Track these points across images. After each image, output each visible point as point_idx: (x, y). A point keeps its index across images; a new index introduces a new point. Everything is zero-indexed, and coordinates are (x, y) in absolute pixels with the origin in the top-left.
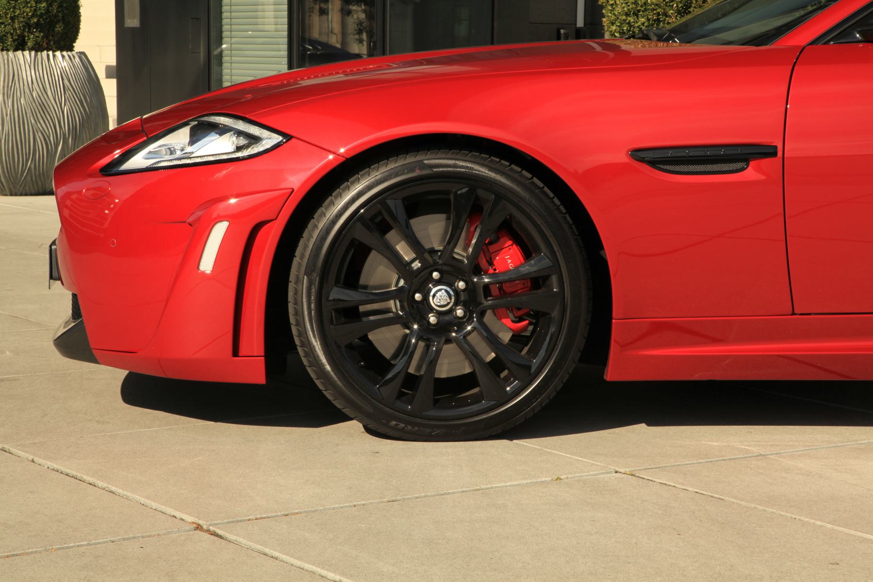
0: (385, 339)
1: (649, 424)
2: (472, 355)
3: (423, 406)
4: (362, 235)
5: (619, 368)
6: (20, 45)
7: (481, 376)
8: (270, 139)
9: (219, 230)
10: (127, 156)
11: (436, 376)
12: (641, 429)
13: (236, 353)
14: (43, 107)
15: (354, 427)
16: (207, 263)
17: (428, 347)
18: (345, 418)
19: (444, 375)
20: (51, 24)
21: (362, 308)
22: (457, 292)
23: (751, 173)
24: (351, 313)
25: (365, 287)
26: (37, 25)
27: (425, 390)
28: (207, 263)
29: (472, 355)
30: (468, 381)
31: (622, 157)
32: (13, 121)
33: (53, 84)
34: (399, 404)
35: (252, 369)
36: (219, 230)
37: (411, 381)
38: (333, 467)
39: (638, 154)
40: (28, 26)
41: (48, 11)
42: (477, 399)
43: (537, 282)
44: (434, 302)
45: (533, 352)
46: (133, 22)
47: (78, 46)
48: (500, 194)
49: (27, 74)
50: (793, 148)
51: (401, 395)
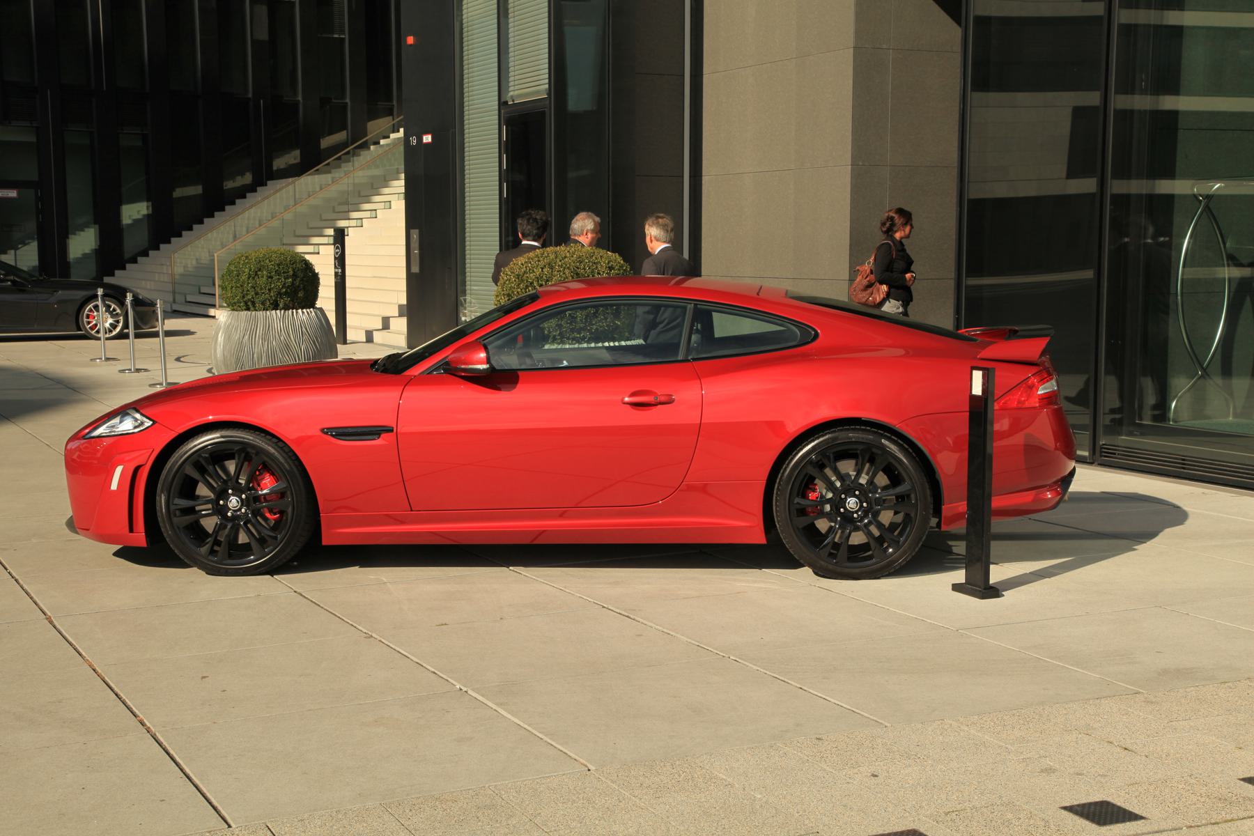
3: (225, 556)
5: (330, 537)
6: (275, 307)
8: (148, 423)
9: (119, 470)
11: (145, 545)
13: (131, 530)
14: (287, 346)
16: (114, 486)
20: (296, 292)
21: (197, 508)
25: (198, 497)
26: (286, 293)
27: (843, 552)
28: (114, 486)
32: (268, 356)
33: (294, 331)
36: (119, 470)
38: (191, 587)
40: (280, 294)
41: (293, 283)
42: (870, 557)
43: (282, 495)
44: (230, 505)
46: (415, 269)
47: (318, 304)
48: (259, 451)
49: (278, 325)
50: (403, 428)
51: (831, 554)
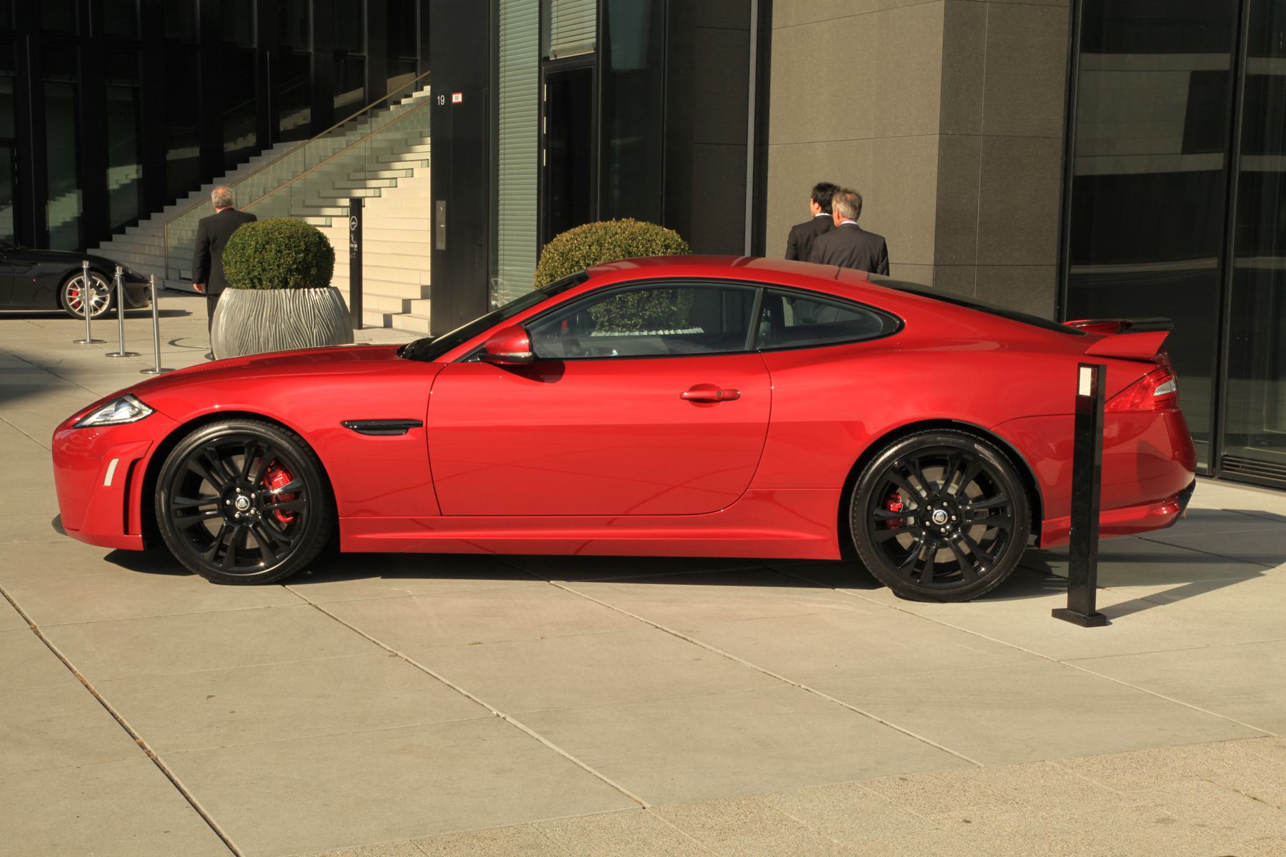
0: (905, 540)
1: (384, 576)
2: (958, 551)
4: (894, 478)
7: (962, 563)
10: (82, 420)
12: (377, 580)
13: (126, 532)
15: (886, 592)
16: (108, 481)
17: (928, 548)
18: (881, 585)
19: (943, 561)
21: (201, 508)
22: (251, 500)
23: (405, 437)
24: (882, 524)
25: (202, 495)
27: (928, 571)
28: (108, 481)
29: (958, 551)
30: (952, 566)
31: (337, 425)
34: (215, 564)
35: (834, 554)
37: (920, 564)
38: (192, 596)
39: (347, 424)
42: (959, 578)
44: (238, 506)
45: (994, 552)
50: (433, 423)
51: (914, 573)
